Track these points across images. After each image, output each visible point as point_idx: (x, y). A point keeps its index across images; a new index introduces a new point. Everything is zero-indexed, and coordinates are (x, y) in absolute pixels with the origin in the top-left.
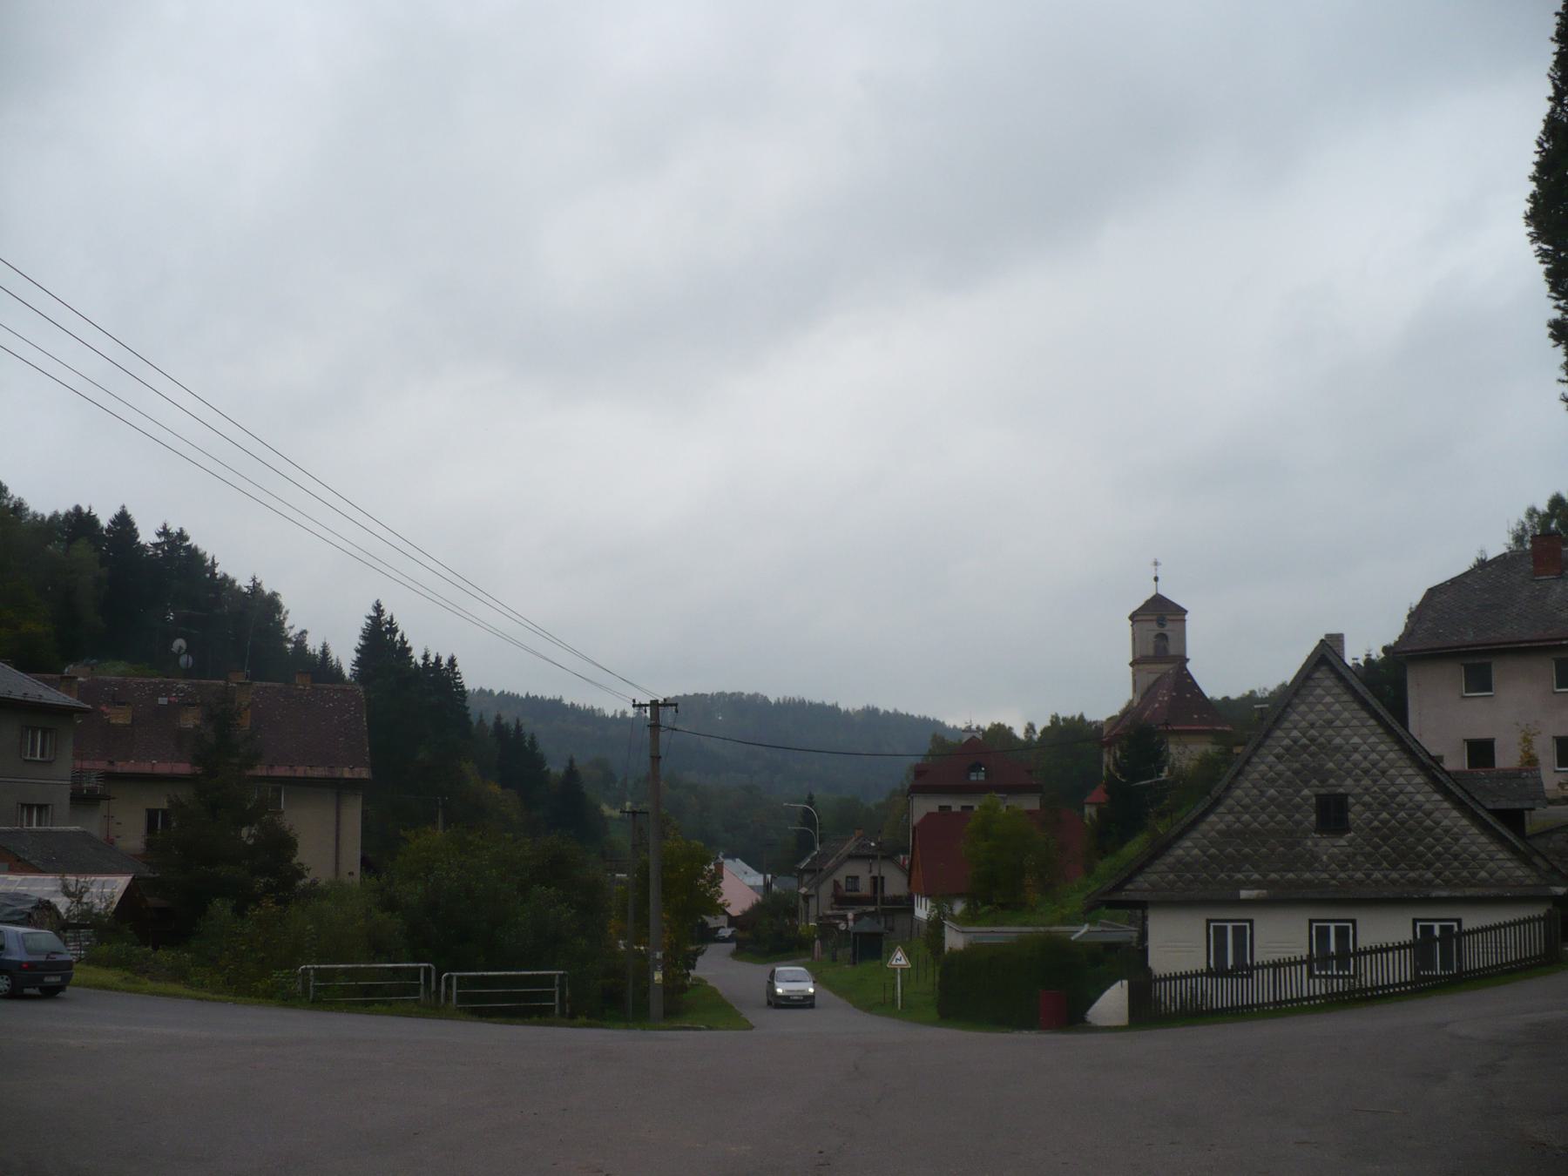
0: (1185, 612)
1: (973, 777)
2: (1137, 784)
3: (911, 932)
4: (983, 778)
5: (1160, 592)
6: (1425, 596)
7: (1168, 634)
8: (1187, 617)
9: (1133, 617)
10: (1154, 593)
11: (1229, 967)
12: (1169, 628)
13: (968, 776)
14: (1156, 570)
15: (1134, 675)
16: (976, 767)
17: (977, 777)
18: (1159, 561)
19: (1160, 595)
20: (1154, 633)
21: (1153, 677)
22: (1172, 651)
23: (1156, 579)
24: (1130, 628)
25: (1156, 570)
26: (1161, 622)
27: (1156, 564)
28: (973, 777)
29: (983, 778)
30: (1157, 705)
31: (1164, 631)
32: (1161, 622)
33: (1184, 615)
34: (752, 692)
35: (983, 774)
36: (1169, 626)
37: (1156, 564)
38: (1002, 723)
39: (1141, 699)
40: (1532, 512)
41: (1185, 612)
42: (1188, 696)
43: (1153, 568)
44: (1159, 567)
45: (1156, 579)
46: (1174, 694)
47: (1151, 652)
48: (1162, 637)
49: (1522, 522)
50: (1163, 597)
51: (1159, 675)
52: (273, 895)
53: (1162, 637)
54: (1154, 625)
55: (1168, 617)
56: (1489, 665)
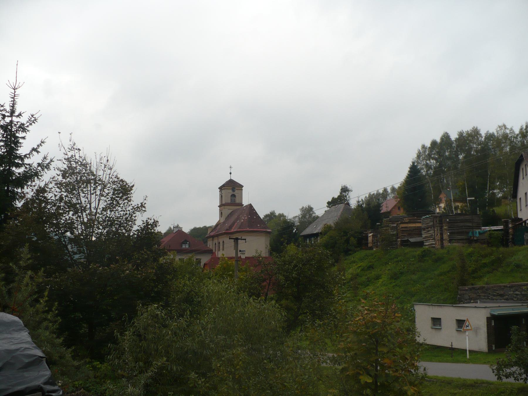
1: (184, 247)
4: (187, 247)
5: (232, 178)
7: (236, 194)
9: (221, 188)
11: (523, 319)
12: (236, 192)
13: (182, 246)
14: (231, 170)
15: (220, 210)
16: (185, 242)
17: (186, 246)
18: (232, 166)
20: (231, 194)
21: (231, 211)
22: (237, 201)
23: (231, 173)
24: (219, 192)
25: (231, 170)
27: (231, 167)
29: (188, 247)
30: (242, 221)
31: (234, 193)
34: (493, 129)
35: (188, 245)
36: (236, 191)
38: (281, 213)
40: (423, 147)
42: (255, 217)
43: (230, 169)
44: (232, 169)
45: (231, 173)
46: (249, 216)
47: (229, 202)
48: (233, 196)
49: (419, 150)
51: (232, 210)
52: (109, 345)
53: (233, 196)
54: (231, 191)
55: (236, 188)
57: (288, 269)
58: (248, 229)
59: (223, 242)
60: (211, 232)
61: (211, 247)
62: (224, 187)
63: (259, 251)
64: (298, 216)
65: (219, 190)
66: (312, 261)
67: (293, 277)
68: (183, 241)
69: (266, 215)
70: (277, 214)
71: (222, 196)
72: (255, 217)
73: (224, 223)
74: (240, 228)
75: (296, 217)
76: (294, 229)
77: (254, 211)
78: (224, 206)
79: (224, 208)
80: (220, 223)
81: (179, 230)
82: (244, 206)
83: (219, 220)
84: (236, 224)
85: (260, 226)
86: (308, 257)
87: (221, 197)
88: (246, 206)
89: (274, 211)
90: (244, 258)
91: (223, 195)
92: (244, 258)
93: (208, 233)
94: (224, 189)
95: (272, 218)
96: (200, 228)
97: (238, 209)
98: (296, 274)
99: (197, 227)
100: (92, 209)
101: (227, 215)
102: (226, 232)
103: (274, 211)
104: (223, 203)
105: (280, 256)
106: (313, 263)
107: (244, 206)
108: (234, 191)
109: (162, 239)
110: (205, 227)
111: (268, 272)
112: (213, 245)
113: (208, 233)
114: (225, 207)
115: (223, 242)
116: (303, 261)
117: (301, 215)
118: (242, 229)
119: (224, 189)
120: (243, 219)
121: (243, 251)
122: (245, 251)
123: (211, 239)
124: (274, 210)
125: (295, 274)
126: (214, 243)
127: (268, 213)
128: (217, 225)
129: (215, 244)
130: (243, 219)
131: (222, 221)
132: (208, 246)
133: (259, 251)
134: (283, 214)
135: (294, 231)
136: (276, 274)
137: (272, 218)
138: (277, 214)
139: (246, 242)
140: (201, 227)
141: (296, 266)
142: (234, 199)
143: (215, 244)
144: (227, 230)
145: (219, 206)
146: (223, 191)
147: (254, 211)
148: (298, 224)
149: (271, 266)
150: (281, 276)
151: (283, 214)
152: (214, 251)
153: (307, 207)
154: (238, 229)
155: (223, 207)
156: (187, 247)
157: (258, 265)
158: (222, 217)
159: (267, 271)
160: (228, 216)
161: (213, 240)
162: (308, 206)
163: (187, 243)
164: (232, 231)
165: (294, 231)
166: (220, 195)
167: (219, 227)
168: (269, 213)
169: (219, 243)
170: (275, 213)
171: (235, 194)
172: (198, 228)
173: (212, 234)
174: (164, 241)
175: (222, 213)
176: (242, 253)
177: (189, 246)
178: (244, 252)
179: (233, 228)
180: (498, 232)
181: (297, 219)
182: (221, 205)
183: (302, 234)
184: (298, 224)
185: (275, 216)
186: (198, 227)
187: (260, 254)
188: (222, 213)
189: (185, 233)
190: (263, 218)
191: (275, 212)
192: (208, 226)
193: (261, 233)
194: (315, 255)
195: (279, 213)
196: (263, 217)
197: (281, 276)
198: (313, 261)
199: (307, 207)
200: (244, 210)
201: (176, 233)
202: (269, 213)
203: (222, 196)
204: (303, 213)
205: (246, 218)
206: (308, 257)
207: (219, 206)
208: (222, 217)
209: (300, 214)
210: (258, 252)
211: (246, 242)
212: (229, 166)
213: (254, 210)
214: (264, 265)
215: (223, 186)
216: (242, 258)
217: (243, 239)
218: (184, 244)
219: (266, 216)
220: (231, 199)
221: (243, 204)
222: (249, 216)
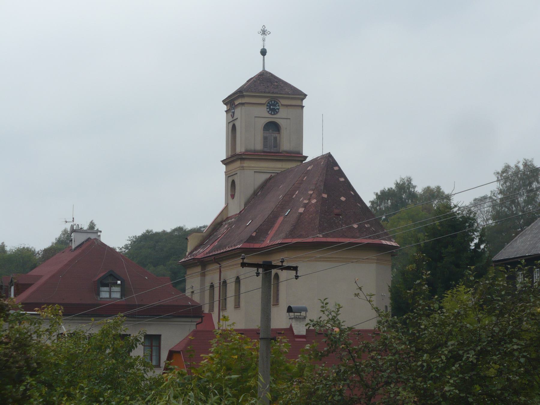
0: (304, 96)
2: (239, 376)
3: (290, 143)
5: (267, 69)
6: (365, 203)
8: (305, 102)
10: (259, 70)
13: (98, 293)
15: (228, 175)
18: (268, 28)
19: (267, 73)
21: (263, 177)
22: (286, 145)
23: (264, 52)
26: (273, 109)
27: (264, 32)
28: (104, 294)
30: (301, 210)
32: (273, 109)
33: (302, 99)
35: (118, 289)
36: (283, 112)
37: (264, 32)
38: (433, 186)
39: (246, 205)
41: (304, 96)
42: (343, 199)
43: (260, 37)
44: (267, 37)
45: (264, 52)
46: (325, 196)
47: (259, 146)
50: (272, 75)
51: (268, 176)
54: (263, 111)
56: (271, 271)
57: (429, 369)
58: (320, 238)
59: (238, 280)
60: (196, 249)
61: (196, 298)
62: (243, 96)
63: (331, 307)
64: (490, 198)
65: (225, 108)
66: (511, 342)
67: (444, 396)
68: (102, 274)
69: (383, 192)
70: (419, 190)
71: (234, 128)
72: (343, 199)
73: (241, 217)
74: (292, 234)
75: (484, 198)
76: (472, 240)
77: (342, 179)
78: (242, 159)
79: (242, 168)
80: (228, 218)
81: (89, 239)
82: (308, 160)
83: (226, 208)
84: (281, 219)
85: (361, 227)
86: (496, 329)
87: (233, 130)
88: (315, 161)
89: (409, 180)
90: (304, 333)
91: (238, 124)
92: (304, 333)
93: (189, 250)
94: (243, 104)
95: (404, 204)
96: (164, 232)
97: (285, 173)
98: (455, 386)
99: (154, 231)
100: (385, 365)
101: (250, 191)
102: (248, 246)
103: (409, 180)
104: (240, 149)
105: (404, 323)
106: (515, 347)
107: (308, 160)
108: (273, 111)
109: (32, 269)
110: (180, 229)
111: (360, 375)
112: (202, 291)
113: (189, 250)
114: (246, 164)
115: (238, 280)
116: (480, 340)
117: (501, 192)
118: (301, 236)
119: (243, 104)
120: (305, 206)
121: (300, 310)
122: (305, 310)
123: (199, 269)
124: (409, 175)
125: (452, 385)
126: (207, 285)
127: (390, 184)
128: (217, 225)
129: (212, 286)
130: (305, 206)
131: (234, 210)
132: (188, 293)
133: (331, 307)
134: (438, 188)
135: (472, 246)
136: (387, 383)
137: (404, 204)
138: (419, 190)
139: (297, 277)
140: (169, 230)
141: (455, 357)
142: (275, 138)
143: (212, 286)
144: (251, 239)
145: (223, 162)
146: (238, 112)
147: (342, 179)
148: (490, 222)
149: (372, 358)
150: (404, 389)
151: (438, 188)
152: (206, 310)
153: (522, 167)
154: (286, 238)
155: (238, 164)
156: (116, 295)
157: (328, 352)
158: (233, 196)
159: (358, 372)
160: (255, 194)
161: (203, 275)
162: (525, 165)
163: (116, 284)
164: (268, 242)
165: (472, 246)
166: (228, 123)
167: (223, 230)
168: (394, 187)
169: (225, 282)
170: (414, 187)
171: (279, 121)
172: (157, 234)
173: (201, 253)
174: (39, 277)
175: (233, 182)
176: (296, 318)
177: (123, 294)
178: (303, 314)
179: (271, 233)
180: (259, 221)
181: (487, 207)
182: (232, 156)
183: (503, 255)
184: (490, 222)
185: (413, 196)
186: (157, 228)
187: (333, 314)
188: (233, 182)
189: (112, 250)
190: (372, 203)
191: (414, 183)
192: (189, 227)
193: (333, 249)
194: (520, 320)
195: (425, 186)
196: (373, 197)
197: (404, 389)
198: (514, 340)
199: (522, 167)
200: (307, 173)
201: (80, 251)
202: (394, 187)
203: (234, 128)
204: (509, 188)
205: (314, 201)
206: (496, 329)
207: (223, 162)
208: (233, 196)
209: (497, 191)
210: (328, 306)
211: (297, 277)
212: (260, 28)
213: (340, 173)
214: (350, 352)
215: (240, 93)
216: (296, 332)
217: (289, 268)
218: (106, 285)
219: (383, 196)
220: (265, 139)
221: (304, 154)
222: (325, 196)
